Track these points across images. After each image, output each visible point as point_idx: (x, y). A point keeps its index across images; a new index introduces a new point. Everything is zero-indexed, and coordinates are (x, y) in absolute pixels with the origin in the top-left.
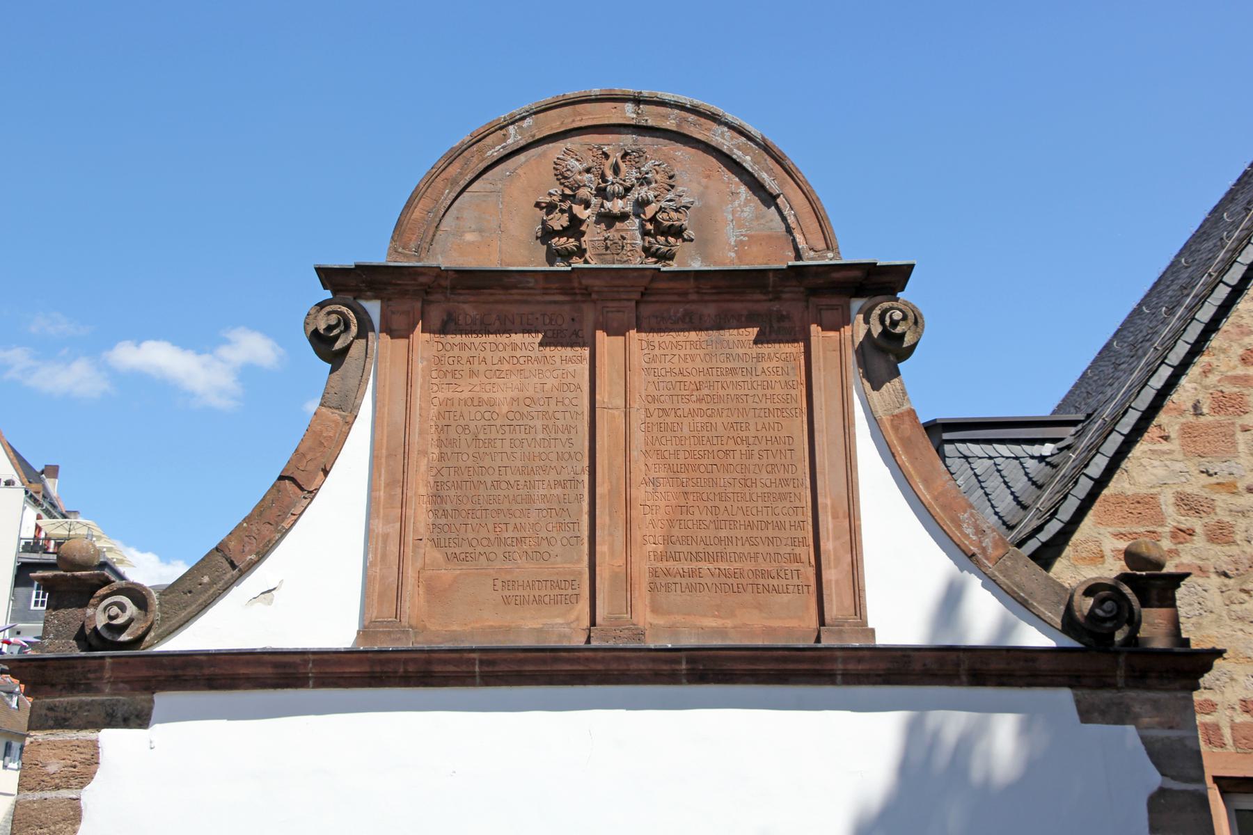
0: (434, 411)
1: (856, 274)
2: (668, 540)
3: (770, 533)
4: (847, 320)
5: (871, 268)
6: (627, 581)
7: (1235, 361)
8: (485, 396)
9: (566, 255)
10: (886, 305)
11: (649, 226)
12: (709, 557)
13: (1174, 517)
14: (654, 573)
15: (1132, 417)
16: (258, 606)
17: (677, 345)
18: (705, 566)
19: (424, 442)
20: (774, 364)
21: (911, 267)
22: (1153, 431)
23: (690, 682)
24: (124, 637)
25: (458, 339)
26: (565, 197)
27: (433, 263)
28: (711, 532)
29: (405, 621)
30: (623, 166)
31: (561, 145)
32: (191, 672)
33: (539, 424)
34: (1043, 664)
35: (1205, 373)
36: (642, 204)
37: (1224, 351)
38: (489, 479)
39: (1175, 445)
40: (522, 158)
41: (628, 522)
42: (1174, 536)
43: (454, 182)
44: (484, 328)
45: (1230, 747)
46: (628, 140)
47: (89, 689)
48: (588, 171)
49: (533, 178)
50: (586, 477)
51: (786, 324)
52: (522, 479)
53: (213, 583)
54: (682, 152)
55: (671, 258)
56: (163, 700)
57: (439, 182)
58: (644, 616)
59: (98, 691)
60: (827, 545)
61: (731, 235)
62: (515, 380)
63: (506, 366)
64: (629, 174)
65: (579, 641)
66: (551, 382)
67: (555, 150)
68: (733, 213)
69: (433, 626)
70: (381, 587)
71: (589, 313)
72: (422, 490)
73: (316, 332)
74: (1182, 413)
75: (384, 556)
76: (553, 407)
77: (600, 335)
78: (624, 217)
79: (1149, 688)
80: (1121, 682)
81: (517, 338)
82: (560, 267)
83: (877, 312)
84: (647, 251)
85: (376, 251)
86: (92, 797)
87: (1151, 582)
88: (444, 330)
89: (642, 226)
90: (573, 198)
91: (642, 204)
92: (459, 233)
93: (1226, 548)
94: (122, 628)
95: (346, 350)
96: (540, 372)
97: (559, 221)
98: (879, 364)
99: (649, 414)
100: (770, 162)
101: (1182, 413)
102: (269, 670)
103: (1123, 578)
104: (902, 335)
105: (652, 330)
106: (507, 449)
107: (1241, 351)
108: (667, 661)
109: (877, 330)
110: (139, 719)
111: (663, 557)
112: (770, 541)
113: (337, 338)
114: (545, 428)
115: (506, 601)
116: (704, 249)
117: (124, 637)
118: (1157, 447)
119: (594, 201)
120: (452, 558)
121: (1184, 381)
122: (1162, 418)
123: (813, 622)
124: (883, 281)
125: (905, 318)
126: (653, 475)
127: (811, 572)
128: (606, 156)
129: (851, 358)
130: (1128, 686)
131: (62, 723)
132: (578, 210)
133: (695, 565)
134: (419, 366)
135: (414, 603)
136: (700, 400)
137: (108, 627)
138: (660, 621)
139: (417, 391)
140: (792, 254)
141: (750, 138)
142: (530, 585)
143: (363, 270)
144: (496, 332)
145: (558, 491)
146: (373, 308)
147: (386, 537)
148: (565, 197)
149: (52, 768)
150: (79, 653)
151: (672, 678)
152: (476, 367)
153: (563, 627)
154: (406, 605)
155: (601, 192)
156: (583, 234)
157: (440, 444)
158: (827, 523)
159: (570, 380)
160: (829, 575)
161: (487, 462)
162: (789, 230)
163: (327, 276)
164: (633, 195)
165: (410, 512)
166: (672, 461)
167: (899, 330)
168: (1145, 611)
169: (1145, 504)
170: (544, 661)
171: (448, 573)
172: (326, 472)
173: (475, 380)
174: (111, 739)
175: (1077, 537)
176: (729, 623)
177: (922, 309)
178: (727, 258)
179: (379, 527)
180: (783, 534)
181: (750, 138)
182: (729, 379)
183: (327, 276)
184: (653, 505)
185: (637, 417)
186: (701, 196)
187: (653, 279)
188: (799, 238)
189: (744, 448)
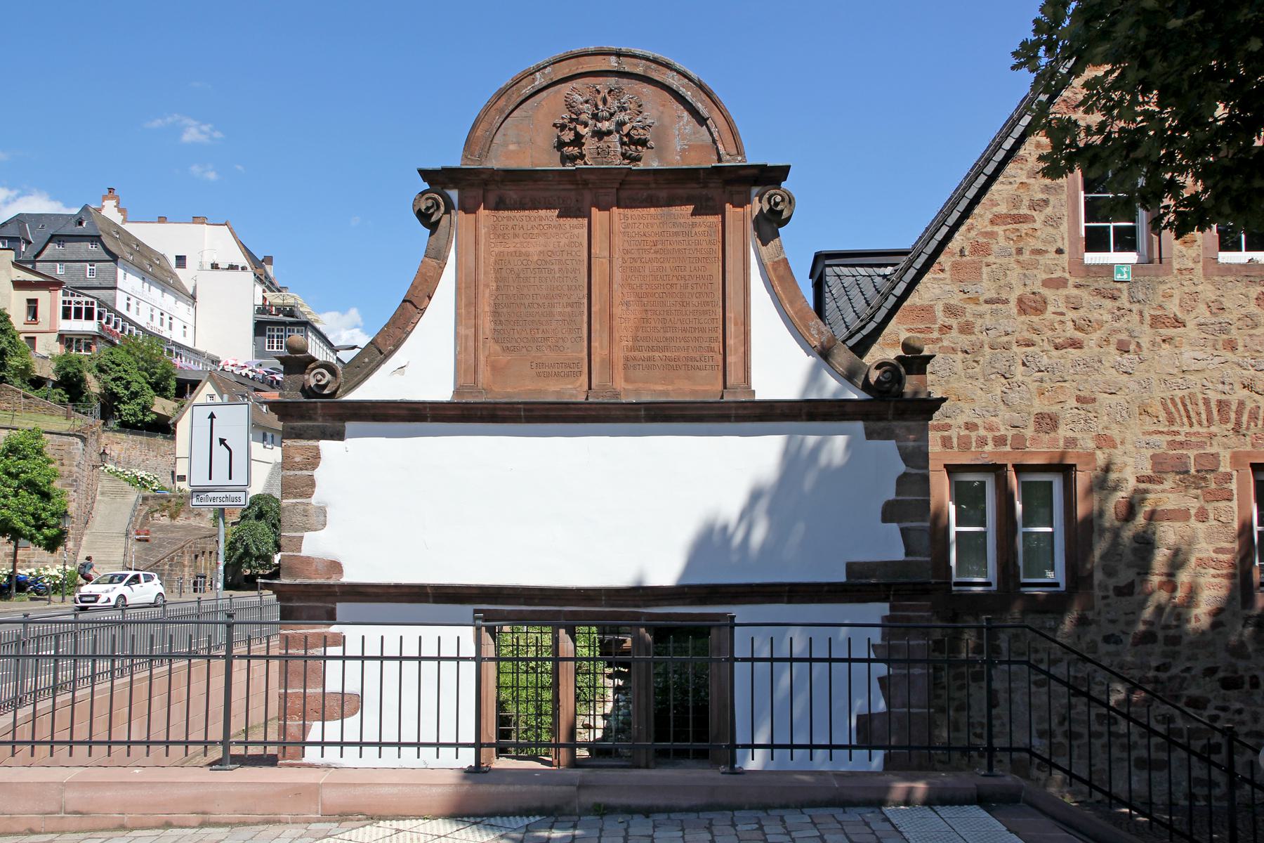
0: (492, 260)
1: (755, 171)
2: (635, 339)
3: (697, 335)
4: (749, 201)
5: (763, 168)
6: (609, 363)
7: (987, 222)
8: (523, 250)
9: (573, 159)
10: (772, 192)
11: (625, 139)
12: (659, 349)
13: (941, 318)
14: (627, 359)
15: (923, 258)
16: (397, 376)
17: (642, 217)
18: (657, 354)
19: (487, 278)
20: (703, 229)
21: (789, 167)
22: (936, 267)
23: (647, 421)
24: (326, 392)
25: (506, 213)
26: (572, 120)
27: (489, 165)
28: (661, 334)
29: (480, 385)
30: (609, 99)
31: (570, 85)
32: (363, 412)
33: (556, 267)
34: (849, 409)
35: (969, 230)
36: (621, 124)
37: (981, 216)
38: (526, 302)
39: (947, 275)
40: (544, 94)
41: (611, 329)
42: (940, 330)
43: (502, 111)
44: (521, 206)
45: (956, 449)
46: (612, 81)
47: (310, 419)
48: (587, 102)
49: (551, 107)
50: (585, 301)
51: (710, 203)
52: (546, 302)
53: (370, 362)
54: (647, 89)
55: (639, 160)
56: (350, 426)
57: (492, 112)
58: (620, 384)
59: (316, 420)
60: (731, 342)
61: (677, 144)
62: (542, 240)
63: (536, 231)
64: (613, 104)
65: (581, 398)
66: (564, 241)
67: (566, 88)
68: (679, 130)
69: (496, 389)
70: (465, 366)
71: (588, 196)
72: (487, 309)
73: (420, 210)
74: (953, 255)
75: (466, 349)
76: (565, 257)
77: (594, 210)
78: (609, 133)
79: (906, 420)
80: (890, 417)
81: (542, 213)
82: (569, 167)
83: (766, 196)
84: (623, 155)
85: (455, 160)
86: (318, 474)
87: (915, 361)
88: (497, 208)
89: (621, 139)
90: (577, 120)
91: (621, 124)
92: (506, 144)
93: (969, 337)
94: (324, 387)
95: (438, 222)
96: (557, 234)
97: (568, 136)
98: (767, 228)
99: (624, 261)
100: (704, 96)
101: (953, 255)
102: (405, 412)
103: (899, 358)
104: (782, 211)
105: (626, 207)
106: (537, 283)
107: (991, 216)
108: (632, 410)
109: (766, 208)
110: (339, 436)
111: (633, 349)
112: (697, 339)
113: (432, 214)
114: (560, 270)
115: (538, 375)
116: (660, 154)
117: (326, 392)
118: (937, 276)
119: (590, 122)
120: (506, 350)
121: (956, 235)
122: (942, 258)
123: (720, 387)
124: (773, 176)
125: (783, 200)
126: (626, 299)
127: (720, 357)
128: (599, 92)
129: (750, 226)
130: (894, 419)
131: (299, 436)
132: (580, 128)
133: (651, 354)
134: (483, 231)
135: (484, 376)
136: (656, 252)
137: (316, 385)
138: (630, 387)
139: (482, 247)
140: (715, 158)
141: (690, 80)
142: (552, 366)
143: (446, 171)
144: (529, 209)
145: (569, 309)
146: (454, 194)
147: (466, 337)
148: (572, 120)
149: (297, 459)
150: (303, 400)
151: (636, 419)
152: (517, 231)
153: (573, 390)
154: (480, 377)
155: (595, 116)
156: (583, 144)
157: (497, 280)
158: (731, 328)
159: (575, 239)
160: (731, 359)
161: (525, 291)
162: (714, 141)
163: (425, 174)
164: (615, 119)
165: (480, 322)
166: (639, 290)
167: (779, 208)
168: (908, 377)
169: (927, 311)
170: (561, 410)
171: (504, 359)
172: (430, 298)
173: (517, 240)
174: (326, 446)
175: (886, 331)
176: (670, 388)
177: (794, 194)
178: (675, 160)
179: (463, 331)
180: (705, 335)
181: (690, 80)
182: (674, 239)
183: (425, 174)
184: (626, 317)
185: (617, 263)
186: (659, 119)
187: (627, 175)
188: (721, 147)
189: (682, 282)
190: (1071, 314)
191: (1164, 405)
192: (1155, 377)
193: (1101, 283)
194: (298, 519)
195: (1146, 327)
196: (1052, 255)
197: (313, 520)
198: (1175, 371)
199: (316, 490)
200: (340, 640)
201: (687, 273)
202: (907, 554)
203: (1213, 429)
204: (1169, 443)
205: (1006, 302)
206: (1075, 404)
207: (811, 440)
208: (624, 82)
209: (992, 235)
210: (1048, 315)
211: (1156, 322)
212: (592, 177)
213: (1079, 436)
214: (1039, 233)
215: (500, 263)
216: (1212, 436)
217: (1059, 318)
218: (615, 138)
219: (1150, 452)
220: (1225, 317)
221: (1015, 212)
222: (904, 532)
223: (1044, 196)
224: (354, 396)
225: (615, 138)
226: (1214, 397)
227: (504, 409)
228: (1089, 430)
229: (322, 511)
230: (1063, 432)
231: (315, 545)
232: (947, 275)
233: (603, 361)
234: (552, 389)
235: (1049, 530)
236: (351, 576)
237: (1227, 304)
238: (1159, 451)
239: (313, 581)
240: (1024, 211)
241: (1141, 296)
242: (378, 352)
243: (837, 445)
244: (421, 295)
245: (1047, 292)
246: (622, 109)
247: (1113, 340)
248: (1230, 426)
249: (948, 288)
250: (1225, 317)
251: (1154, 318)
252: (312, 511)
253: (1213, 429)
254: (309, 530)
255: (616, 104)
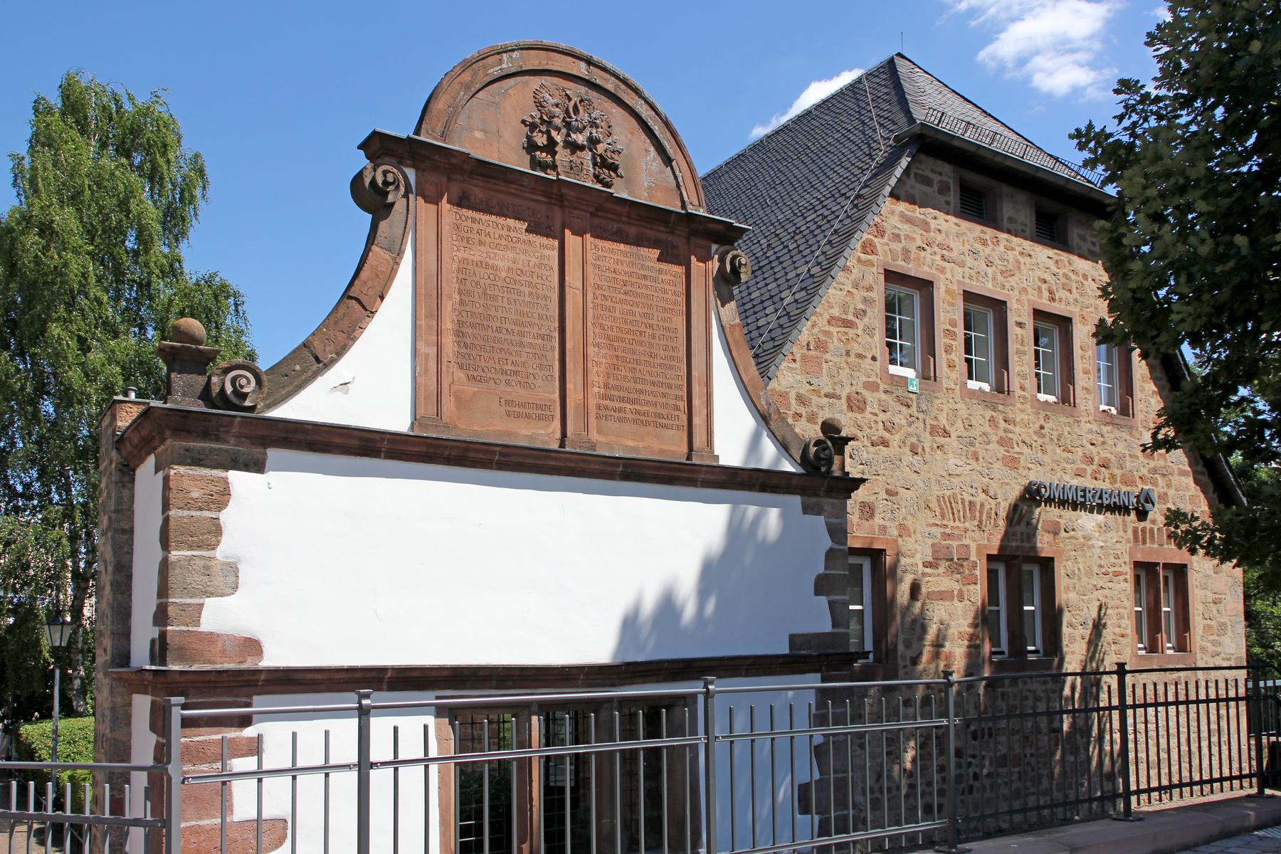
2: (606, 386)
7: (825, 322)
8: (491, 262)
9: (544, 166)
16: (338, 393)
18: (628, 406)
19: (450, 288)
25: (470, 213)
33: (526, 290)
38: (494, 325)
40: (511, 81)
43: (467, 87)
47: (218, 439)
48: (557, 106)
53: (303, 371)
54: (616, 110)
56: (273, 454)
58: (594, 436)
59: (225, 441)
60: (696, 402)
62: (510, 254)
63: (503, 242)
66: (534, 261)
67: (536, 82)
70: (427, 392)
78: (582, 148)
79: (831, 497)
81: (511, 222)
83: (729, 256)
86: (226, 517)
106: (505, 304)
112: (664, 395)
114: (530, 294)
115: (508, 414)
117: (248, 403)
120: (471, 378)
123: (685, 449)
127: (685, 417)
135: (449, 405)
141: (657, 113)
142: (523, 405)
144: (497, 214)
145: (539, 342)
149: (195, 494)
152: (483, 238)
158: (696, 389)
159: (546, 262)
161: (493, 312)
162: (678, 186)
171: (471, 388)
172: (382, 298)
173: (482, 248)
176: (641, 445)
181: (657, 113)
182: (643, 282)
190: (882, 416)
191: (938, 501)
192: (933, 478)
193: (900, 392)
194: (196, 579)
195: (927, 435)
196: (869, 361)
197: (218, 581)
198: (945, 474)
199: (224, 539)
200: (255, 748)
201: (655, 322)
202: (834, 626)
203: (967, 524)
204: (943, 534)
205: (839, 398)
206: (885, 496)
207: (752, 510)
208: (593, 95)
209: (828, 334)
210: (867, 414)
211: (934, 431)
212: (571, 193)
213: (888, 524)
214: (860, 339)
215: (464, 268)
216: (966, 530)
217: (874, 418)
218: (587, 155)
219: (930, 542)
220: (971, 433)
221: (844, 317)
222: (831, 604)
223: (863, 307)
224: (279, 413)
225: (587, 155)
226: (967, 498)
227: (478, 451)
228: (893, 519)
229: (232, 569)
230: (878, 520)
231: (220, 616)
232: (797, 365)
233: (577, 406)
234: (525, 432)
235: (859, 607)
236: (275, 657)
237: (974, 423)
238: (936, 541)
239: (218, 667)
240: (850, 317)
241: (925, 408)
242: (313, 359)
243: (771, 518)
244: (370, 293)
245: (866, 393)
246: (593, 124)
247: (908, 443)
248: (976, 523)
249: (798, 377)
250: (971, 433)
251: (932, 427)
252: (217, 569)
253: (967, 524)
254: (212, 594)
255: (587, 118)
